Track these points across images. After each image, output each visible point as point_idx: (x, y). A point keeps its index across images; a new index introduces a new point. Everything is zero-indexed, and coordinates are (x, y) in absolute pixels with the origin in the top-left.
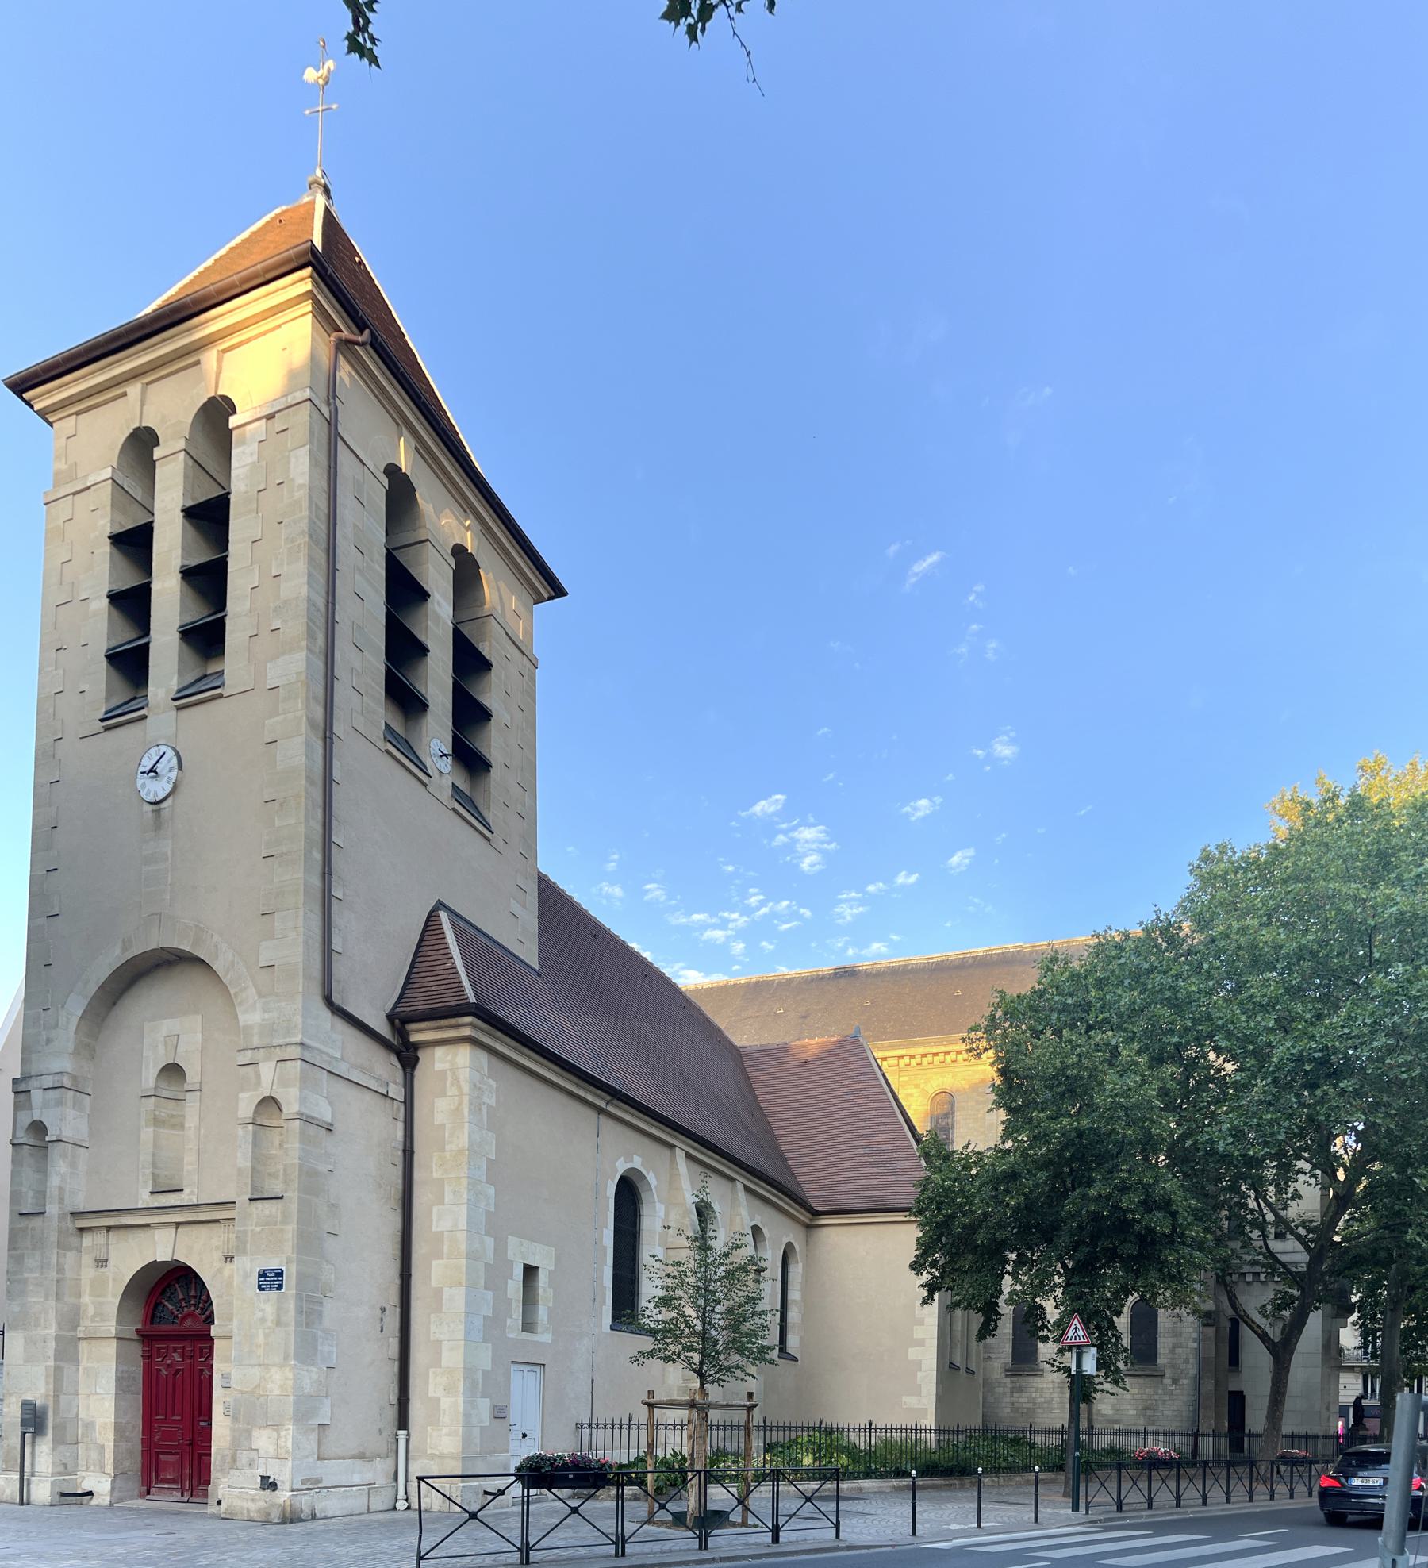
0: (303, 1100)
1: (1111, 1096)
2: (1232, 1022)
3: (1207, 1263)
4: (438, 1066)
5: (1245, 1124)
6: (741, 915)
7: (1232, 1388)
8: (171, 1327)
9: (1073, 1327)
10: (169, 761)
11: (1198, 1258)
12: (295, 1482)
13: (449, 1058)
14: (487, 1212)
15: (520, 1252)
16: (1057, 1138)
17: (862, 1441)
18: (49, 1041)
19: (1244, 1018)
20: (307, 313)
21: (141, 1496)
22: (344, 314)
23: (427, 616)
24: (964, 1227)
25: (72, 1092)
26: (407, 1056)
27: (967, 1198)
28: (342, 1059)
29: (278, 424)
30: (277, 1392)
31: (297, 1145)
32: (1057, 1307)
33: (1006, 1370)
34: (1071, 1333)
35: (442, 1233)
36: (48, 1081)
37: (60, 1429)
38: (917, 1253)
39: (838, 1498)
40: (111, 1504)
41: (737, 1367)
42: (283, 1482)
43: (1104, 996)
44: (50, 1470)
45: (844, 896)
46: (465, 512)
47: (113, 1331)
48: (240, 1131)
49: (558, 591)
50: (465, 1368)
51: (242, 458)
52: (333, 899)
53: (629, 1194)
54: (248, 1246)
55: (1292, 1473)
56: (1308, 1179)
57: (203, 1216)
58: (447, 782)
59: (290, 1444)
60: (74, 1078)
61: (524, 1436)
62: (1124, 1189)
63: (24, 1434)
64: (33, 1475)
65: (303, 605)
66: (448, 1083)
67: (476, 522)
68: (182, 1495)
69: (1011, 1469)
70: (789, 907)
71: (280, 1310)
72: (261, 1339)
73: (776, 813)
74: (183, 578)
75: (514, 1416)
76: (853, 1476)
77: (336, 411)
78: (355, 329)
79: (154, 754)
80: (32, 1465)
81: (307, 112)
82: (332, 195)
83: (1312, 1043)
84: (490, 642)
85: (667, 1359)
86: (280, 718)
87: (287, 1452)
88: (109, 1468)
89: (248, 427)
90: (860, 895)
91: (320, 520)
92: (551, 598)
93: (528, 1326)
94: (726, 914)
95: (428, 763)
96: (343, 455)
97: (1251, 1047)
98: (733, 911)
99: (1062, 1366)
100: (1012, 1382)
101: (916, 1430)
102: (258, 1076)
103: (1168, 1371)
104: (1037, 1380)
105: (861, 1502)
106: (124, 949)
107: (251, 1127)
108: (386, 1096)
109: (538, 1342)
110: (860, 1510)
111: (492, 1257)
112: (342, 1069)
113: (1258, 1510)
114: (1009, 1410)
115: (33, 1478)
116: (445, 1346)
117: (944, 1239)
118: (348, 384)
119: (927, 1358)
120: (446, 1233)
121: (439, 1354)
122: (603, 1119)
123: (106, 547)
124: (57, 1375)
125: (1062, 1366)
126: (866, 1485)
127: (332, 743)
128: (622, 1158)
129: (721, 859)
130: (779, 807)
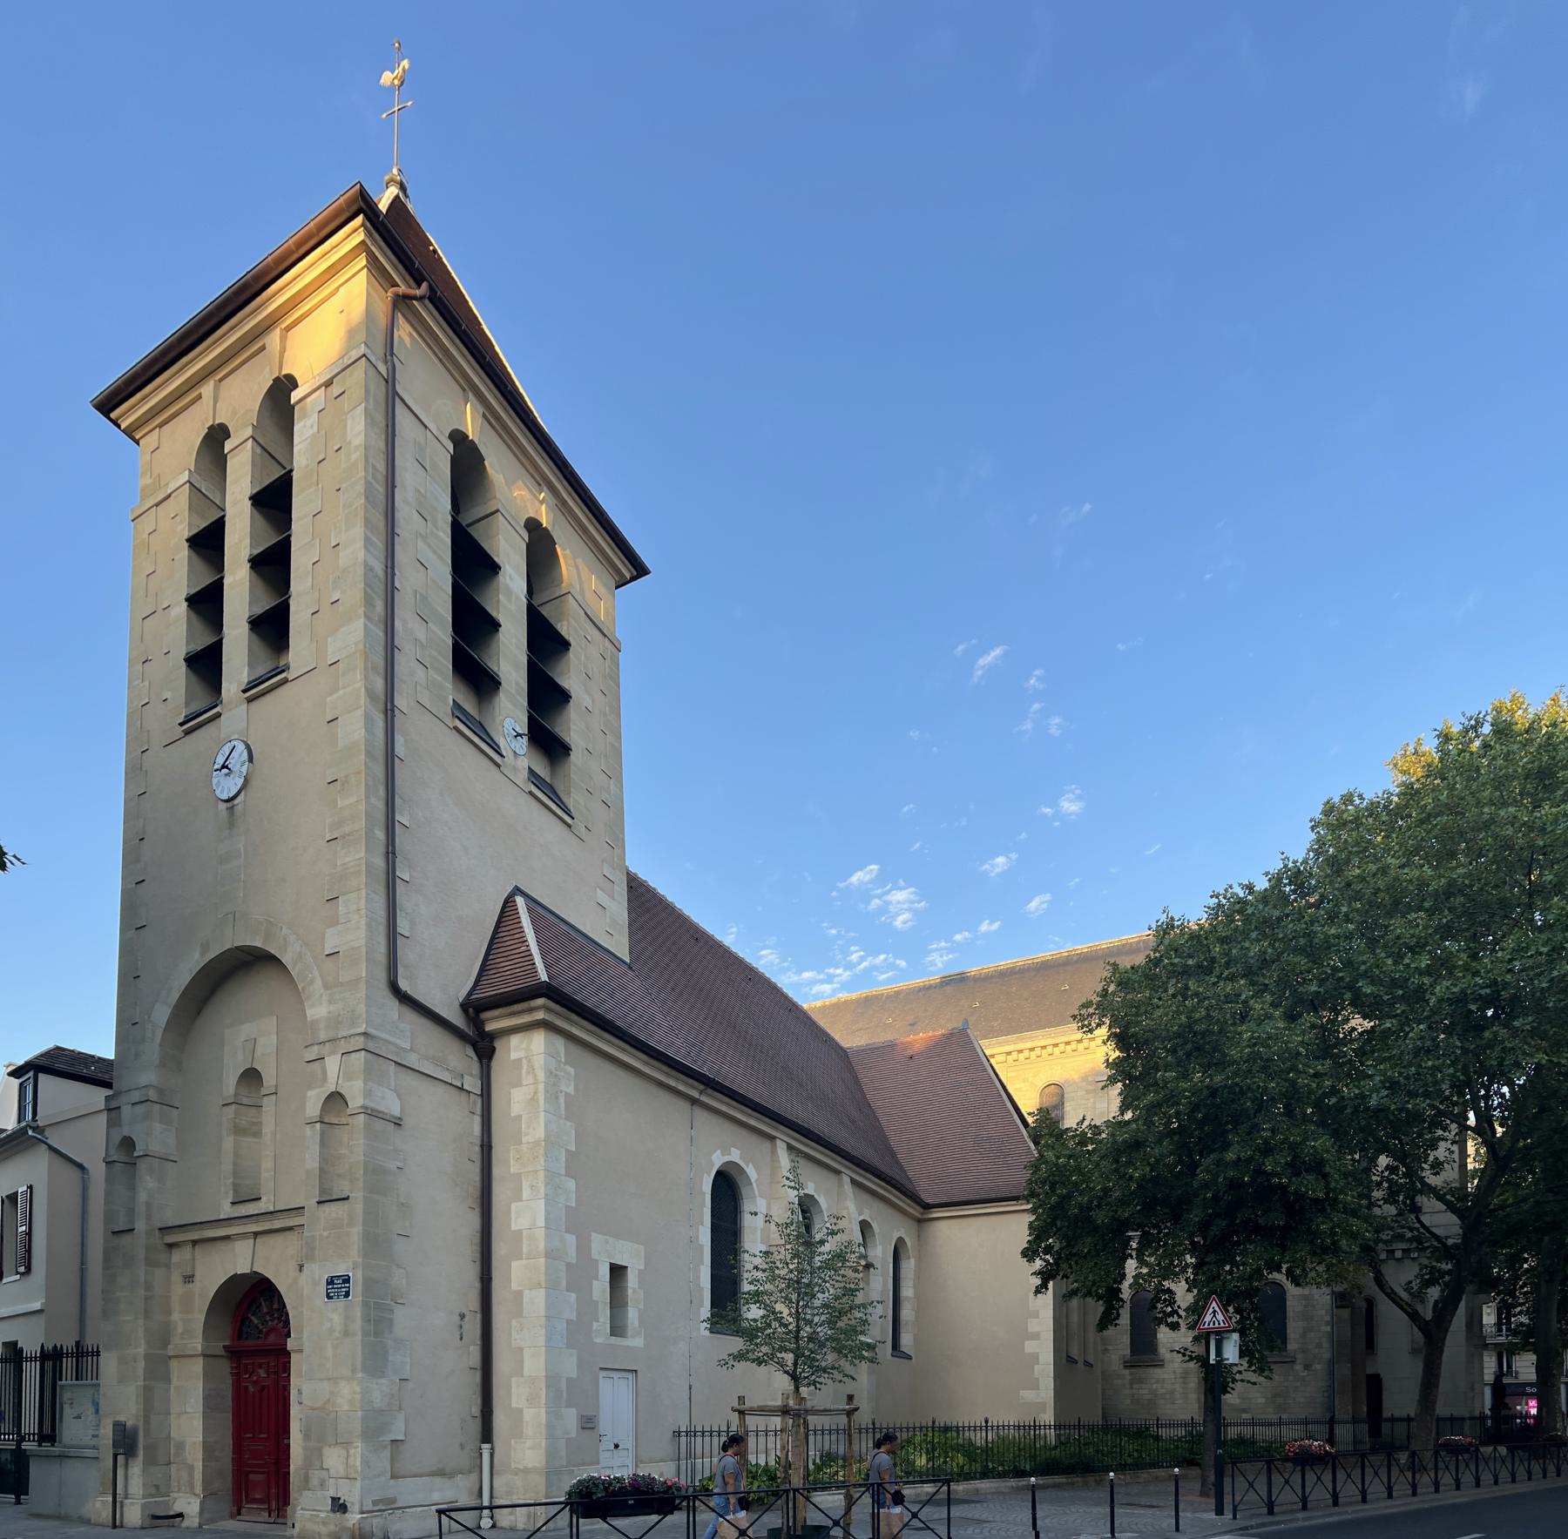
0: (368, 1093)
1: (1249, 1046)
2: (1377, 967)
3: (1367, 1231)
4: (514, 1055)
5: (1400, 1074)
6: (845, 970)
7: (1370, 1371)
8: (260, 1342)
9: (1211, 1310)
10: (240, 756)
11: (1356, 1226)
12: (364, 1504)
13: (524, 1045)
14: (567, 1207)
15: (605, 1251)
16: (1187, 1098)
17: (978, 1439)
18: (137, 1055)
19: (1390, 961)
20: (362, 269)
21: (232, 1517)
22: (401, 267)
23: (498, 589)
24: (1081, 1207)
25: (158, 1106)
26: (483, 1047)
27: (1083, 1175)
28: (412, 1050)
29: (335, 389)
30: (346, 1408)
31: (362, 1141)
32: (1189, 1290)
33: (1125, 1362)
34: (1208, 1318)
35: (520, 1232)
36: (136, 1096)
37: (151, 1450)
38: (1030, 1238)
39: (949, 1502)
40: (200, 1527)
41: (833, 1368)
42: (353, 1503)
43: (1230, 950)
44: (141, 1493)
45: (935, 946)
46: (540, 485)
47: (199, 1347)
48: (308, 1131)
49: (640, 570)
50: (546, 1376)
51: (304, 429)
52: (398, 880)
53: (727, 1189)
54: (317, 1252)
55: (1457, 1461)
56: (1450, 1146)
57: (278, 1224)
58: (524, 763)
59: (358, 1463)
60: (161, 1091)
61: (616, 1446)
62: (1267, 1150)
63: (115, 1456)
64: (126, 1498)
65: (360, 571)
66: (524, 1071)
67: (550, 495)
68: (270, 1516)
69: (1138, 1466)
70: (886, 959)
71: (347, 1318)
72: (329, 1352)
73: (870, 881)
74: (251, 567)
75: (604, 1426)
76: (968, 1477)
77: (393, 370)
78: (412, 283)
79: (227, 749)
80: (126, 1486)
81: (384, 116)
82: (408, 191)
83: (1477, 979)
84: (569, 623)
85: (759, 1362)
86: (341, 692)
87: (357, 1472)
88: (199, 1489)
89: (309, 399)
90: (949, 944)
91: (376, 481)
92: (633, 579)
93: (617, 1329)
94: (831, 971)
95: (502, 743)
96: (401, 414)
97: (1400, 992)
98: (837, 968)
99: (1194, 1355)
100: (1131, 1374)
101: (1035, 1426)
102: (324, 1072)
103: (1299, 1356)
104: (1158, 1371)
105: (978, 1505)
106: (204, 951)
107: (318, 1125)
108: (461, 1089)
109: (628, 1347)
110: (976, 1516)
111: (574, 1255)
112: (412, 1060)
113: (1426, 1506)
114: (1128, 1401)
115: (126, 1501)
116: (527, 1353)
117: (1058, 1223)
118: (408, 345)
119: (1043, 1349)
120: (524, 1232)
121: (520, 1362)
122: (698, 1111)
123: (184, 552)
124: (147, 1394)
125: (1194, 1355)
126: (983, 1485)
127: (393, 716)
128: (719, 1152)
129: (825, 925)
130: (874, 875)
